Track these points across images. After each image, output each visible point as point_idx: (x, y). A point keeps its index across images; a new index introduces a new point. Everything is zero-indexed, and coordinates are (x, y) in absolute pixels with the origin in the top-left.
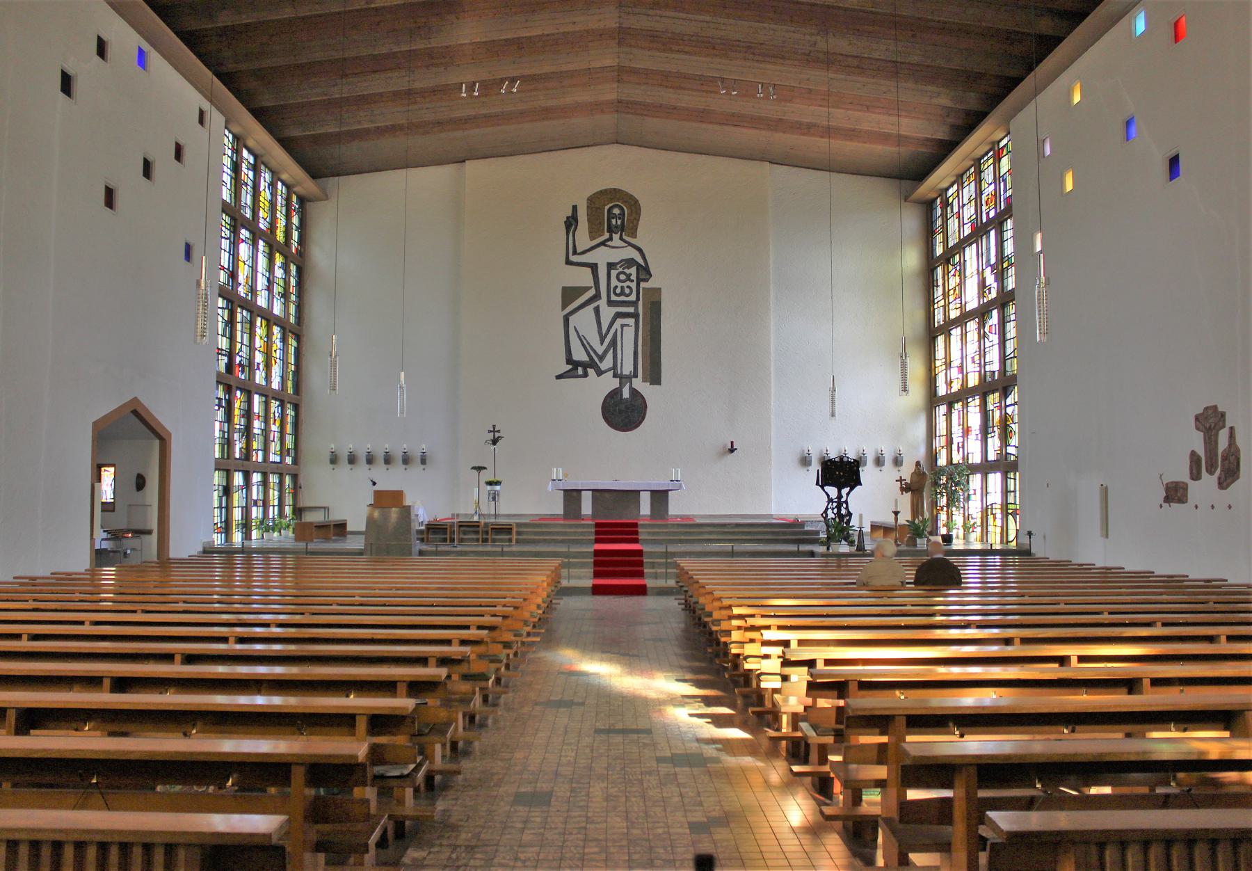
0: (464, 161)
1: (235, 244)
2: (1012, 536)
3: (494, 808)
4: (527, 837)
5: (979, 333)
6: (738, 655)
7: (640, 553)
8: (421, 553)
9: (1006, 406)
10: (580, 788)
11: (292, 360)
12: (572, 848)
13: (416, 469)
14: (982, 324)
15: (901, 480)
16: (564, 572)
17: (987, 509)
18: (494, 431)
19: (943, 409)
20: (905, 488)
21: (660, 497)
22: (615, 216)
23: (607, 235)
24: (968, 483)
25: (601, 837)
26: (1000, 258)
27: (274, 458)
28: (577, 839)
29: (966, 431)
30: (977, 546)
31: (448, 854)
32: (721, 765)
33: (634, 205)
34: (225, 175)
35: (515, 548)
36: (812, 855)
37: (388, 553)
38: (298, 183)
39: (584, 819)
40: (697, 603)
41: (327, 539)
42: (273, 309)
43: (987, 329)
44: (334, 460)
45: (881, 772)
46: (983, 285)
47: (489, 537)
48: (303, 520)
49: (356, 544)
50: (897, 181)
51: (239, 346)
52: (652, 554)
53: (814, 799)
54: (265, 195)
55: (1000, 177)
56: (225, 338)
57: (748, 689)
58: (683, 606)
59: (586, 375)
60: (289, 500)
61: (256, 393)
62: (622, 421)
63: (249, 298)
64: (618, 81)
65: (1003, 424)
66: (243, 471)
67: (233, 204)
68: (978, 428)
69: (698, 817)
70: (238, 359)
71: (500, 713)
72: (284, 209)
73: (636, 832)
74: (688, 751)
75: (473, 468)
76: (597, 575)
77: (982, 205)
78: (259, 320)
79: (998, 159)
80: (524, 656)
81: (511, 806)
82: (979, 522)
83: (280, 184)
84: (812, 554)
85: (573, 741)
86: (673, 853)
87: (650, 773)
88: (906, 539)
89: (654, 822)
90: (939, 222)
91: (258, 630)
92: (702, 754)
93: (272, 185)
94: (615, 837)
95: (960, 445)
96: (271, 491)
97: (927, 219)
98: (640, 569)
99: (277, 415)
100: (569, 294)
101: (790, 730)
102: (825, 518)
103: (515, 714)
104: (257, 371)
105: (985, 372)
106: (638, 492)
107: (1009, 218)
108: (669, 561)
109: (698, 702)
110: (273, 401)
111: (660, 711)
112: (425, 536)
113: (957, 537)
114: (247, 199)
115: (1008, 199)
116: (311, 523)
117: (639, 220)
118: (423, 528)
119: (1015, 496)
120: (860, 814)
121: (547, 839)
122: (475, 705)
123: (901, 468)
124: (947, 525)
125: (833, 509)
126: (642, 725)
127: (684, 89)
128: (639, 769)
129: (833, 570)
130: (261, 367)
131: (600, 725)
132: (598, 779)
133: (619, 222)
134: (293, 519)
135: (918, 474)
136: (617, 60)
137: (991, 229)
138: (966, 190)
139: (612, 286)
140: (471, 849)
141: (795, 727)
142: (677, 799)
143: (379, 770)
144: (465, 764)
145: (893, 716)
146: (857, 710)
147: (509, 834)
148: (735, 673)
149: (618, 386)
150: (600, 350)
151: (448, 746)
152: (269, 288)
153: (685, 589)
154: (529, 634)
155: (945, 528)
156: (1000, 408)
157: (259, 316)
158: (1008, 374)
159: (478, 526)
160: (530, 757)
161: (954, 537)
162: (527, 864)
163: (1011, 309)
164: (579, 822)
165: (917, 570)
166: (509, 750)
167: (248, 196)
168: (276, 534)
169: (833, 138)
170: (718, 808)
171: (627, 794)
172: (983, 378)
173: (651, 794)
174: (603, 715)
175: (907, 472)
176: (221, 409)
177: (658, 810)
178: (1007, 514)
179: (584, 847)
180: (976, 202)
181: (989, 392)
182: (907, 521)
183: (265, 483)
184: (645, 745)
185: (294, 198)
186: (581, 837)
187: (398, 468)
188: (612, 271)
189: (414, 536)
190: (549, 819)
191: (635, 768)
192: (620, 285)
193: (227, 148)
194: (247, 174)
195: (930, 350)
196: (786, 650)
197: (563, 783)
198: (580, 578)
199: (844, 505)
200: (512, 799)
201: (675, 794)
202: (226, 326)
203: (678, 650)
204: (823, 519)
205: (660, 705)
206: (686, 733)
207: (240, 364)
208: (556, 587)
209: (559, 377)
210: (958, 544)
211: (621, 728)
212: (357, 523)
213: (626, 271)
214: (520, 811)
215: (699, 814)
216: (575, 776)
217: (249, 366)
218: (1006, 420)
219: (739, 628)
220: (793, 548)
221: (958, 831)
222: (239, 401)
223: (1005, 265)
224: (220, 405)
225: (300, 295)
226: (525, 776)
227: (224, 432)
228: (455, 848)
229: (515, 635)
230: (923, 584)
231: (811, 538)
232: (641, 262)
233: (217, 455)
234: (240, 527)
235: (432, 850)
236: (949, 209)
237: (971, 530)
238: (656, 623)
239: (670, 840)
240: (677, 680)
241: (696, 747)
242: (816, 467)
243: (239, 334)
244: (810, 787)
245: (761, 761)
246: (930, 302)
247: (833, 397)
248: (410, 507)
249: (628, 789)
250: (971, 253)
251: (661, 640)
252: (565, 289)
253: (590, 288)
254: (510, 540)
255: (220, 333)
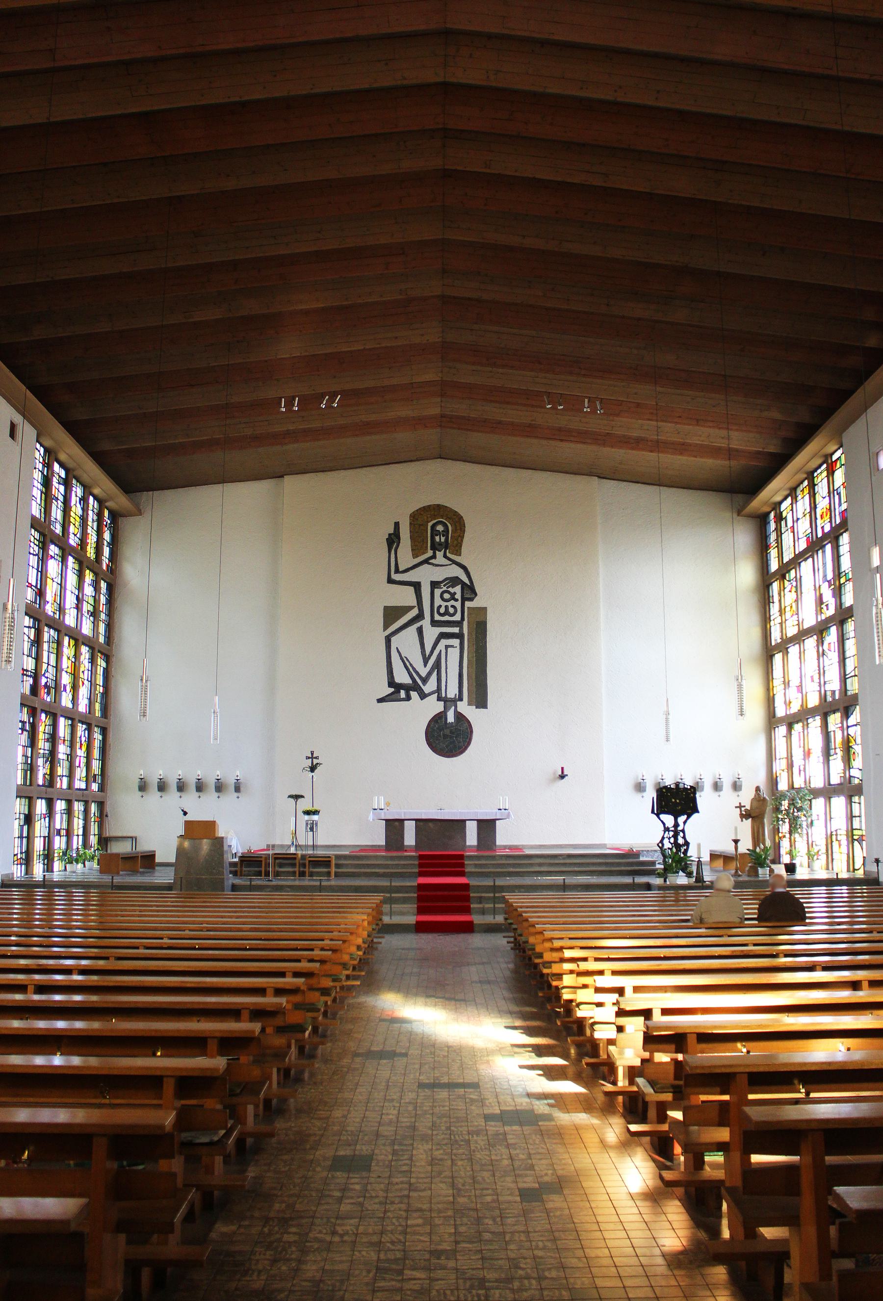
0: (282, 476)
1: (43, 560)
2: (859, 863)
3: (310, 1174)
4: (345, 1208)
5: (818, 651)
6: (571, 1001)
7: (466, 887)
8: (234, 888)
9: (848, 727)
10: (402, 1150)
11: (100, 680)
12: (394, 1220)
13: (230, 797)
14: (821, 641)
15: (740, 807)
16: (386, 908)
17: (831, 835)
18: (312, 758)
19: (782, 730)
20: (746, 815)
21: (487, 827)
22: (438, 533)
23: (430, 553)
24: (811, 809)
25: (425, 1207)
26: (837, 573)
27: (80, 784)
28: (400, 1210)
29: (807, 754)
30: (822, 875)
31: (260, 1228)
32: (553, 1123)
33: (459, 522)
34: (35, 489)
35: (334, 882)
36: (651, 1226)
37: (199, 889)
38: (111, 498)
39: (406, 1186)
40: (527, 942)
41: (134, 872)
42: (81, 628)
43: (826, 646)
44: (143, 787)
45: (723, 1134)
46: (820, 601)
47: (307, 870)
48: (109, 851)
49: (164, 877)
50: (729, 494)
51: (45, 666)
52: (479, 888)
53: (654, 1160)
54: (76, 510)
55: (834, 490)
56: (30, 658)
57: (582, 1038)
58: (513, 945)
59: (408, 698)
60: (94, 829)
61: (62, 716)
62: (447, 747)
63: (57, 616)
64: (442, 396)
65: (846, 746)
66: (45, 799)
67: (43, 520)
68: (820, 750)
69: (529, 1182)
70: (44, 681)
71: (317, 1066)
72: (95, 524)
73: (461, 1200)
74: (518, 1108)
75: (290, 796)
76: (420, 911)
77: (816, 519)
78: (66, 639)
79: (831, 472)
80: (342, 1001)
81: (329, 1171)
82: (824, 850)
83: (91, 498)
84: (648, 887)
85: (395, 1097)
86: (502, 1225)
87: (478, 1133)
88: (747, 869)
89: (482, 1189)
90: (773, 537)
91: (58, 977)
92: (533, 1110)
93: (84, 500)
94: (440, 1206)
95: (802, 768)
96: (76, 820)
97: (761, 534)
98: (467, 904)
99: (83, 739)
100: (391, 614)
101: (627, 1083)
102: (661, 848)
103: (333, 1067)
104: (64, 693)
105: (825, 691)
106: (464, 821)
107: (845, 532)
108: (497, 895)
109: (529, 1052)
110: (79, 724)
111: (488, 1062)
112: (238, 869)
113: (801, 865)
114: (57, 513)
115: (843, 513)
116: (117, 855)
117: (463, 537)
118: (237, 860)
119: (861, 822)
120: (702, 1179)
121: (368, 1210)
122: (290, 1059)
123: (740, 793)
124: (790, 853)
125: (669, 838)
126: (469, 1078)
127: (508, 403)
128: (466, 1129)
129: (669, 906)
130: (68, 688)
131: (423, 1079)
132: (422, 1140)
133: (443, 539)
134: (98, 849)
135: (759, 799)
136: (440, 375)
137: (827, 544)
138: (800, 503)
139: (436, 605)
140: (284, 1222)
141: (632, 1082)
142: (506, 1162)
143: (186, 1136)
144: (280, 1124)
145: (735, 1074)
146: (696, 1067)
147: (328, 1203)
148: (567, 1019)
149: (442, 709)
150: (424, 672)
151: (261, 1107)
152: (78, 607)
153: (514, 926)
154: (348, 977)
155: (788, 856)
156: (842, 728)
157: (66, 635)
158: (849, 693)
159: (295, 858)
160: (349, 1116)
161: (798, 866)
162: (346, 1238)
163: (850, 626)
164: (401, 1190)
165: (760, 905)
166: (326, 1108)
167: (59, 511)
168: (80, 866)
169: (662, 452)
170: (550, 1172)
171: (454, 1157)
172: (823, 698)
173: (478, 1156)
174: (427, 1066)
175: (746, 798)
176: (24, 732)
177: (486, 1174)
178: (853, 840)
179: (407, 1218)
180: (811, 516)
181: (830, 712)
182: (748, 850)
183: (69, 811)
184: (472, 1100)
185: (106, 513)
186: (403, 1206)
187: (211, 796)
188: (436, 590)
189: (227, 869)
190: (369, 1187)
191: (461, 1126)
192: (444, 604)
193: (37, 461)
194: (58, 489)
195: (768, 670)
196: (620, 999)
197: (384, 1145)
198: (402, 914)
199: (681, 834)
200: (330, 1163)
201: (504, 1157)
202: (32, 645)
203: (507, 994)
204: (659, 849)
205: (488, 1055)
206: (515, 1087)
207: (46, 686)
208: (377, 925)
209: (380, 701)
210: (802, 874)
211: (447, 1081)
212: (166, 853)
213: (450, 589)
214: (337, 1178)
215: (530, 1179)
216: (398, 1137)
217: (56, 688)
218: (848, 741)
219: (572, 972)
220: (628, 880)
221: (807, 1203)
222: (43, 724)
223: (843, 580)
224: (23, 729)
225: (110, 614)
226: (343, 1138)
227: (27, 757)
228: (267, 1220)
229: (334, 980)
230: (766, 920)
231: (647, 869)
232: (466, 580)
233: (20, 781)
234: (42, 857)
235: (242, 1223)
236: (783, 523)
237: (815, 858)
238: (483, 963)
239: (500, 1209)
240: (507, 1027)
241: (526, 1103)
242: (651, 794)
243: (45, 654)
244: (649, 1147)
245: (596, 1117)
246: (766, 619)
247: (667, 719)
248: (222, 838)
249: (454, 1151)
250: (806, 566)
251: (489, 982)
252: (386, 609)
253: (413, 607)
254: (329, 874)
255: (26, 653)
